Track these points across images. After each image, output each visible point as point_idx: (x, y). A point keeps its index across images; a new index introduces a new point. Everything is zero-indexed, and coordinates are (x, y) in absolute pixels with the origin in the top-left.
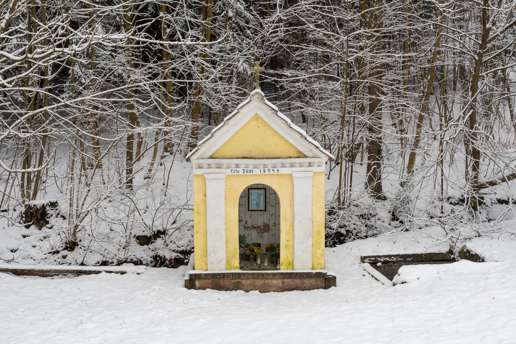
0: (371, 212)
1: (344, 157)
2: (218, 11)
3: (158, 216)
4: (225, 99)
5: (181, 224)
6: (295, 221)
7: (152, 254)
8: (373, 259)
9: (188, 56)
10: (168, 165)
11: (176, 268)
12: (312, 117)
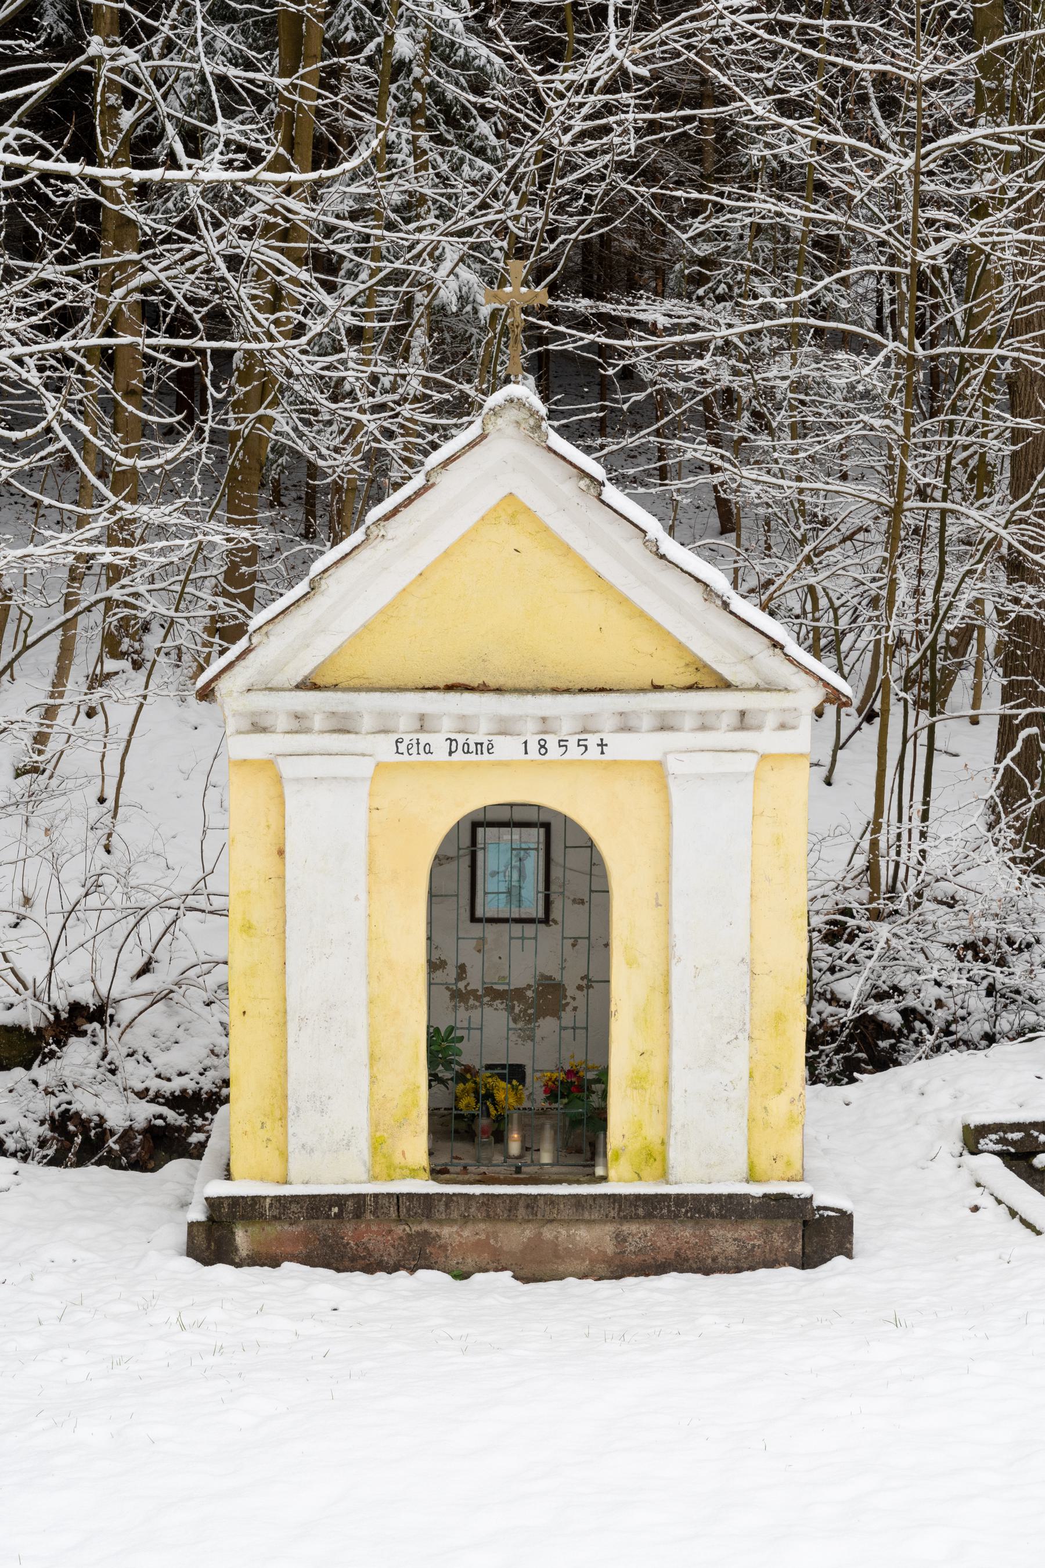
0: (1012, 929)
1: (895, 687)
2: (349, 36)
3: (73, 944)
4: (372, 426)
5: (173, 975)
6: (676, 971)
7: (48, 1106)
8: (1017, 1136)
9: (210, 235)
10: (120, 715)
11: (153, 1170)
12: (761, 511)
